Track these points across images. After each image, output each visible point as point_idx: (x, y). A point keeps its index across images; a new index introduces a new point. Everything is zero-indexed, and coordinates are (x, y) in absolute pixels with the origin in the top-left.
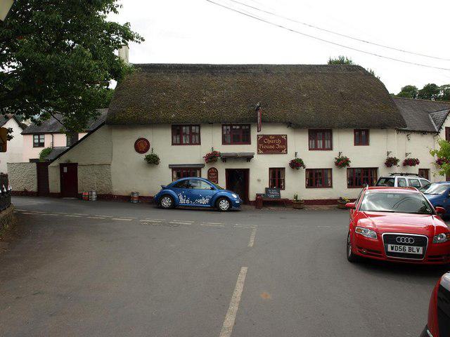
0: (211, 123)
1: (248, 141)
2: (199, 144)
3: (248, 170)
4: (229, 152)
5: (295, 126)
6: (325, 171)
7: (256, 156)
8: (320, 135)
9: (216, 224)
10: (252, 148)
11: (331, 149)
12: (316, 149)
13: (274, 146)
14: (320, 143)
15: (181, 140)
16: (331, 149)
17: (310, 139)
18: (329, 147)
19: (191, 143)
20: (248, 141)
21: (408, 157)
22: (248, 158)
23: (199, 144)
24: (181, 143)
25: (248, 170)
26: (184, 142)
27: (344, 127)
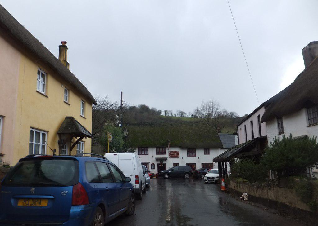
0: (152, 146)
1: (165, 153)
2: (148, 154)
3: (165, 164)
4: (26, 156)
5: (182, 148)
6: (128, 178)
7: (168, 159)
8: (192, 151)
9: (47, 224)
10: (167, 156)
11: (195, 156)
12: (190, 156)
13: (175, 155)
14: (191, 154)
15: (145, 153)
16: (195, 156)
17: (187, 152)
18: (147, 154)
19: (145, 154)
20: (165, 153)
21: (130, 177)
22: (166, 159)
23: (148, 154)
24: (141, 154)
25: (165, 164)
26: (146, 154)
27: (200, 148)
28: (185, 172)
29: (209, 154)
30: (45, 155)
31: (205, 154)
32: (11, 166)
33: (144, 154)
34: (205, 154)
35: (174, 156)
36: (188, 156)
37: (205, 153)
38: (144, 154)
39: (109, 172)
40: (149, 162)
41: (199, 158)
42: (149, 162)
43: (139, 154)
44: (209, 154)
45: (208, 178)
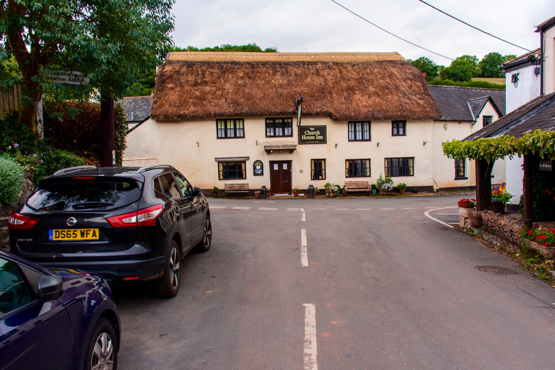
2: (244, 137)
5: (336, 119)
6: (125, 248)
18: (242, 135)
23: (244, 137)
28: (95, 46)
29: (404, 134)
30: (518, 59)
31: (393, 135)
32: (522, 194)
33: (272, 134)
34: (393, 135)
35: (312, 140)
36: (349, 141)
37: (395, 133)
38: (272, 134)
39: (150, 120)
40: (248, 158)
41: (336, 145)
42: (248, 158)
43: (268, 134)
44: (404, 134)
45: (144, 59)
